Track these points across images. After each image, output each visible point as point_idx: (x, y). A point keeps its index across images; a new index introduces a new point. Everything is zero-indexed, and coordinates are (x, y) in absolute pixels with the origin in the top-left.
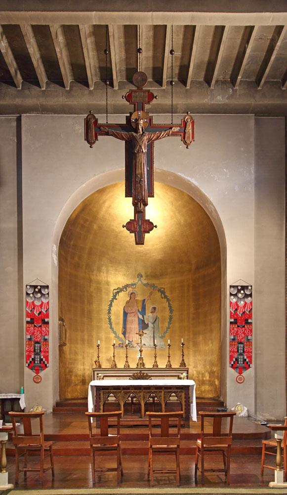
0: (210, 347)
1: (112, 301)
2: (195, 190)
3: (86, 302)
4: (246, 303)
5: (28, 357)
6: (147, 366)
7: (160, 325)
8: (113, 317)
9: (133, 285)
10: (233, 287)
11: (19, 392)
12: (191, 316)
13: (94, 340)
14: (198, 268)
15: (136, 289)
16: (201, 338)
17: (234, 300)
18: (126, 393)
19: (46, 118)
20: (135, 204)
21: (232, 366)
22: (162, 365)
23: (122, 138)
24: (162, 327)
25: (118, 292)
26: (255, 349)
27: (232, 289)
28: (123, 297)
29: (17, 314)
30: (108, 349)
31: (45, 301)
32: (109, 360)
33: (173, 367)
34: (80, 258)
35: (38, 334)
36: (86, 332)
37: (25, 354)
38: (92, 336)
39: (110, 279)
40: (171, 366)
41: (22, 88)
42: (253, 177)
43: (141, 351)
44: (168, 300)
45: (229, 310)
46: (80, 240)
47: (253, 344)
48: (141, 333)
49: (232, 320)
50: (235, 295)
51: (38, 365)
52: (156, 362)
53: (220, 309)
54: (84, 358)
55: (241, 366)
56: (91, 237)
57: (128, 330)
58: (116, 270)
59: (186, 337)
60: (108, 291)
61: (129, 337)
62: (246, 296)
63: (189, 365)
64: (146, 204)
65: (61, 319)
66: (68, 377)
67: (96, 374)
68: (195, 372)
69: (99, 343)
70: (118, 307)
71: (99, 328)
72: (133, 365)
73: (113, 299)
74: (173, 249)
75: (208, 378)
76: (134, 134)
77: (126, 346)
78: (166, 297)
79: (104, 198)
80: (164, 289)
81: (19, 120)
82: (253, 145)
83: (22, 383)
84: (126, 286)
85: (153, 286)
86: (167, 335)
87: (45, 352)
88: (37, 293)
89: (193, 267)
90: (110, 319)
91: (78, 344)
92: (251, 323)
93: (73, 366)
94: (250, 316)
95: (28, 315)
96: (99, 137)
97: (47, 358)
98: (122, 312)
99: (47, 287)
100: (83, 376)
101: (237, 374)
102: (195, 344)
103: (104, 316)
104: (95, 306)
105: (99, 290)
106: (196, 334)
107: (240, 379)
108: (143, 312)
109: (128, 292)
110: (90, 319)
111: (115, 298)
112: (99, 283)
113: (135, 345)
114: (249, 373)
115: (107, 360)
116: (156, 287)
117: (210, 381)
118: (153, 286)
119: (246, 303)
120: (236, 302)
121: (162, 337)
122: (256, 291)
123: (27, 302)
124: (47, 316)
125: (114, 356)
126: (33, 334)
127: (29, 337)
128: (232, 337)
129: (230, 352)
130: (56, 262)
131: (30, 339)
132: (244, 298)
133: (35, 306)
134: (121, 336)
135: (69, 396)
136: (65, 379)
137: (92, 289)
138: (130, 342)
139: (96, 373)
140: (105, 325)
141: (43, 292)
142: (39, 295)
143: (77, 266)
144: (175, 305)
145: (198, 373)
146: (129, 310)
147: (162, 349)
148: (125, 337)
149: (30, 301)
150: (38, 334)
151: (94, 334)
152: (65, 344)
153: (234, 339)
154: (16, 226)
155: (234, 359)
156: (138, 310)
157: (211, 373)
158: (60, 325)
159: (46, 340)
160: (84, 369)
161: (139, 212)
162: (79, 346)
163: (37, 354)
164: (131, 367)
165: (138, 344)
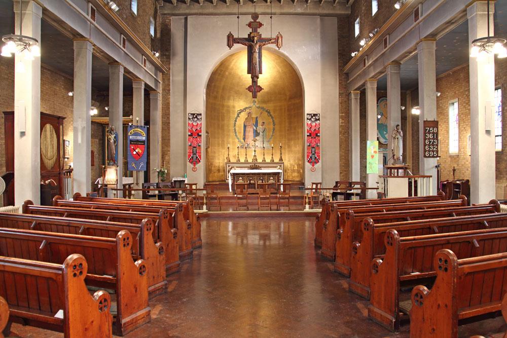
0: (297, 148)
1: (237, 118)
2: (287, 57)
3: (220, 119)
4: (316, 124)
5: (189, 156)
10: (309, 114)
12: (287, 128)
14: (291, 98)
17: (309, 122)
19: (201, 17)
20: (252, 78)
21: (308, 161)
22: (268, 160)
23: (246, 45)
24: (268, 135)
25: (240, 113)
26: (322, 151)
28: (243, 116)
31: (199, 123)
32: (234, 156)
34: (217, 92)
36: (220, 139)
37: (187, 154)
41: (190, 5)
42: (319, 51)
43: (255, 151)
45: (306, 128)
46: (218, 84)
49: (309, 134)
50: (310, 119)
51: (195, 161)
52: (264, 158)
53: (302, 126)
57: (247, 137)
59: (284, 142)
60: (234, 111)
61: (247, 141)
62: (316, 120)
63: (285, 160)
64: (258, 78)
65: (207, 132)
66: (210, 167)
67: (227, 166)
68: (289, 165)
70: (241, 122)
71: (228, 136)
72: (250, 160)
74: (275, 86)
75: (296, 168)
77: (246, 148)
78: (271, 115)
79: (233, 58)
81: (186, 19)
82: (319, 33)
83: (185, 171)
85: (262, 108)
88: (195, 118)
89: (288, 97)
91: (215, 146)
92: (319, 136)
95: (189, 131)
96: (234, 44)
97: (200, 156)
98: (243, 125)
99: (201, 114)
100: (219, 167)
102: (289, 147)
103: (232, 128)
105: (228, 111)
106: (290, 140)
108: (256, 125)
110: (223, 130)
111: (238, 116)
112: (228, 107)
113: (251, 146)
116: (265, 109)
119: (316, 124)
120: (311, 124)
121: (268, 141)
122: (322, 117)
123: (189, 124)
124: (201, 132)
125: (238, 155)
126: (192, 142)
127: (190, 144)
131: (190, 145)
133: (193, 125)
134: (243, 141)
136: (209, 170)
138: (248, 145)
139: (227, 165)
140: (232, 134)
143: (216, 98)
144: (276, 121)
145: (291, 165)
146: (247, 124)
148: (244, 141)
149: (190, 122)
151: (225, 139)
153: (309, 145)
157: (299, 165)
159: (199, 146)
160: (219, 163)
161: (254, 82)
162: (216, 148)
164: (249, 161)
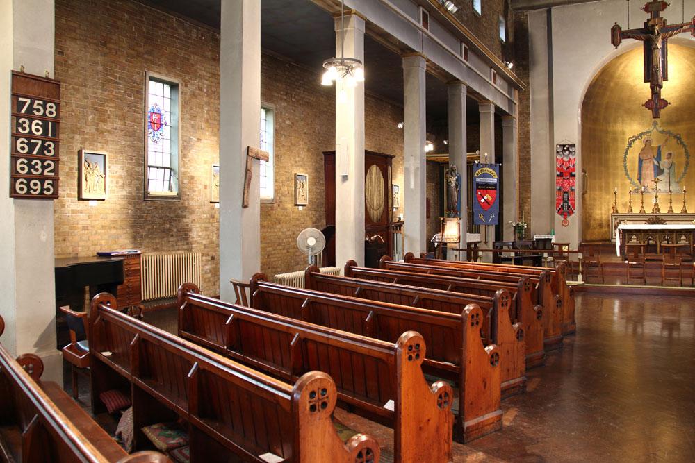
1: (628, 148)
6: (662, 212)
7: (676, 171)
9: (647, 132)
11: (550, 234)
13: (611, 188)
15: (651, 137)
23: (641, 40)
25: (633, 140)
28: (638, 145)
29: (548, 168)
30: (623, 194)
32: (624, 205)
33: (675, 212)
35: (566, 185)
36: (603, 180)
37: (556, 202)
38: (608, 183)
39: (625, 129)
40: (686, 211)
43: (656, 197)
44: (684, 146)
46: (600, 102)
48: (656, 180)
51: (566, 211)
52: (671, 207)
54: (601, 203)
56: (608, 93)
57: (643, 176)
60: (623, 140)
65: (584, 171)
66: (588, 221)
67: (614, 220)
70: (634, 154)
71: (615, 175)
72: (648, 211)
78: (682, 143)
79: (621, 60)
80: (680, 135)
86: (683, 180)
87: (572, 200)
88: (565, 151)
90: (625, 166)
91: (596, 190)
96: (622, 40)
98: (637, 159)
99: (574, 146)
101: (563, 219)
103: (620, 164)
104: (611, 155)
105: (615, 140)
108: (659, 158)
110: (607, 167)
111: (630, 145)
112: (615, 133)
113: (650, 190)
118: (669, 133)
121: (678, 182)
123: (557, 159)
125: (630, 202)
126: (562, 185)
127: (559, 188)
130: (580, 122)
131: (560, 190)
133: (563, 162)
134: (637, 182)
135: (589, 238)
136: (586, 224)
138: (645, 188)
139: (614, 217)
140: (621, 172)
141: (571, 150)
142: (567, 152)
148: (640, 182)
149: (559, 157)
150: (566, 185)
151: (611, 180)
154: (547, 96)
160: (601, 214)
163: (566, 202)
164: (646, 212)
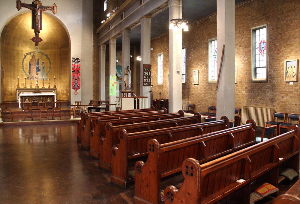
1: (24, 59)
2: (59, 20)
4: (78, 64)
6: (40, 88)
8: (24, 66)
9: (33, 52)
10: (73, 58)
12: (59, 67)
14: (62, 47)
16: (62, 76)
17: (74, 63)
18: (32, 98)
20: (35, 32)
22: (46, 87)
24: (47, 71)
25: (27, 55)
27: (73, 59)
28: (29, 57)
30: (22, 80)
32: (23, 85)
33: (51, 88)
38: (15, 74)
42: (81, 18)
43: (37, 81)
44: (49, 59)
45: (72, 67)
47: (81, 80)
48: (37, 74)
50: (74, 61)
52: (44, 86)
54: (11, 84)
55: (76, 88)
57: (31, 72)
58: (26, 45)
60: (22, 55)
61: (32, 75)
62: (78, 62)
63: (58, 87)
66: (5, 92)
67: (18, 92)
68: (60, 90)
69: (19, 78)
72: (34, 87)
73: (24, 58)
74: (51, 38)
75: (65, 92)
76: (35, 9)
77: (31, 79)
78: (48, 58)
79: (21, 17)
84: (30, 53)
86: (48, 74)
90: (23, 67)
91: (8, 78)
93: (7, 87)
94: (80, 69)
96: (22, 8)
101: (75, 91)
102: (60, 78)
103: (20, 65)
104: (16, 61)
105: (18, 54)
106: (60, 74)
107: (76, 93)
109: (31, 55)
110: (14, 66)
111: (25, 57)
112: (18, 51)
113: (35, 78)
114: (79, 91)
115: (22, 84)
116: (44, 54)
117: (66, 93)
118: (42, 53)
119: (78, 64)
120: (75, 64)
121: (46, 75)
125: (25, 83)
128: (73, 77)
129: (72, 83)
132: (77, 62)
135: (5, 100)
137: (15, 54)
139: (18, 90)
140: (21, 69)
146: (32, 63)
147: (46, 80)
148: (30, 74)
152: (3, 78)
155: (74, 86)
156: (36, 63)
157: (67, 90)
158: (1, 70)
165: (36, 78)
